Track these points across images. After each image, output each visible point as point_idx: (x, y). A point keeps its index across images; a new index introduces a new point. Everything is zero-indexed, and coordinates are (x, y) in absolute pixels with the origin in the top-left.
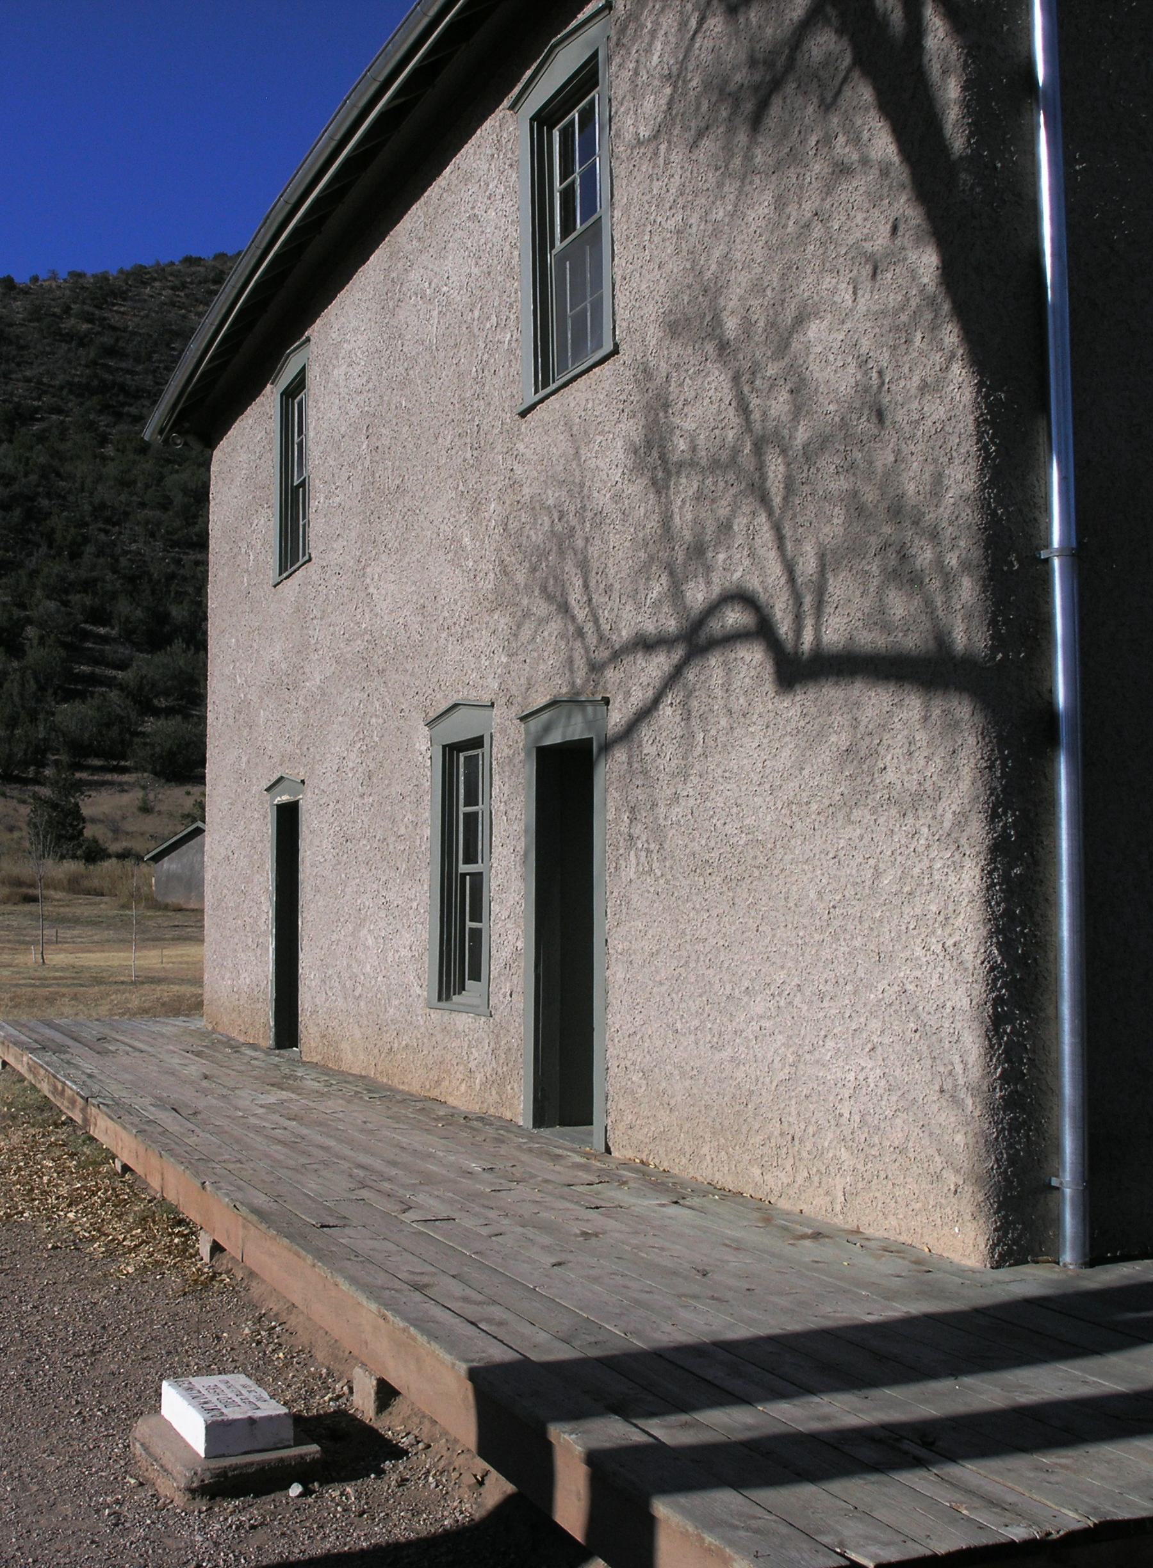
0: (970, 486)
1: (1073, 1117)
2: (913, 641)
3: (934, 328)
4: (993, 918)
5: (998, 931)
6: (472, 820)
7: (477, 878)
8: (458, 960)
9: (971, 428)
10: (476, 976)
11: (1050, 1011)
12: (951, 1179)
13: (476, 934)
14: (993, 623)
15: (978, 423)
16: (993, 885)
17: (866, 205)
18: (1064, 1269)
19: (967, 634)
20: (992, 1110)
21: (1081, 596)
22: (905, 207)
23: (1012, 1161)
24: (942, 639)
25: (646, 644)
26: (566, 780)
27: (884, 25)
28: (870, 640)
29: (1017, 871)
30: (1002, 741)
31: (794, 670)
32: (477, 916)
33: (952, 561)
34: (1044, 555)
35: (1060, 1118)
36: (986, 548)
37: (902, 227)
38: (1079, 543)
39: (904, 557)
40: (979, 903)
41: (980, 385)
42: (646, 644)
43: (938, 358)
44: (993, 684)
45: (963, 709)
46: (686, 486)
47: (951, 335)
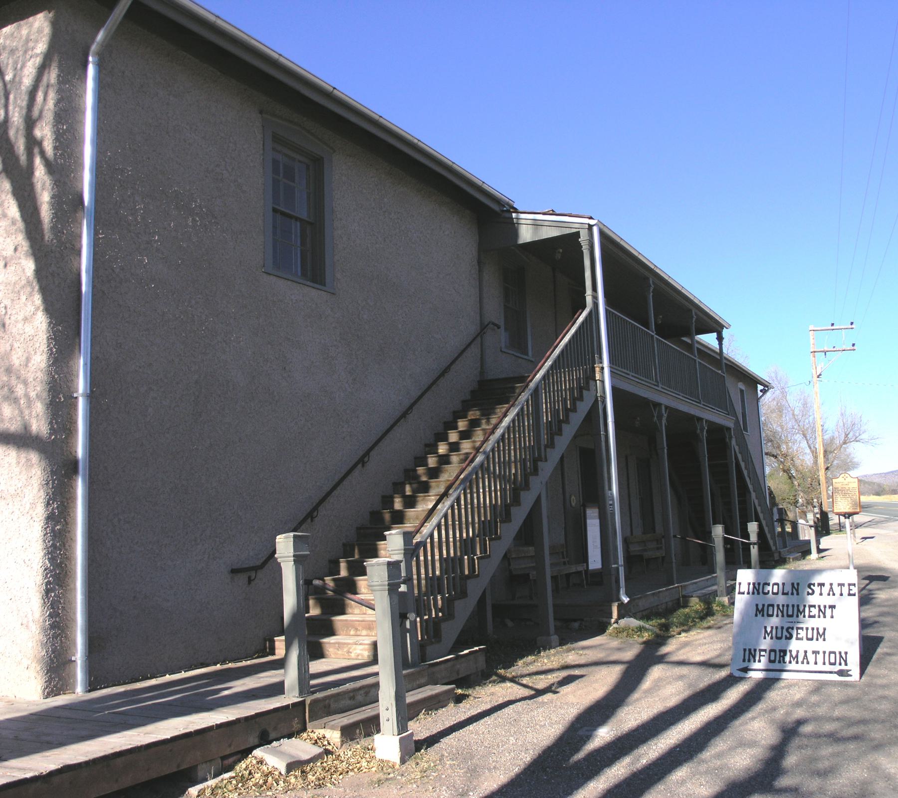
0: (43, 365)
1: (82, 631)
2: (14, 427)
3: (31, 294)
4: (47, 548)
5: (49, 553)
9: (45, 341)
11: (72, 586)
12: (26, 662)
14: (51, 423)
15: (48, 339)
16: (47, 534)
17: (5, 235)
18: (79, 692)
19: (39, 425)
20: (44, 630)
21: (91, 413)
22: (20, 239)
23: (53, 652)
24: (26, 427)
27: (17, 159)
29: (58, 527)
30: (53, 473)
33: (33, 394)
34: (75, 395)
35: (76, 631)
36: (49, 391)
37: (19, 248)
38: (91, 391)
39: (11, 391)
40: (40, 541)
41: (50, 323)
43: (33, 309)
45: (34, 457)
47: (37, 299)
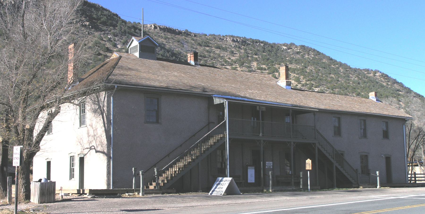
6: (73, 163)
7: (73, 169)
8: (72, 176)
10: (73, 177)
13: (73, 174)
19: (106, 151)
25: (87, 148)
26: (82, 160)
28: (101, 150)
31: (97, 152)
32: (73, 172)
42: (87, 148)
44: (108, 155)
46: (90, 137)
